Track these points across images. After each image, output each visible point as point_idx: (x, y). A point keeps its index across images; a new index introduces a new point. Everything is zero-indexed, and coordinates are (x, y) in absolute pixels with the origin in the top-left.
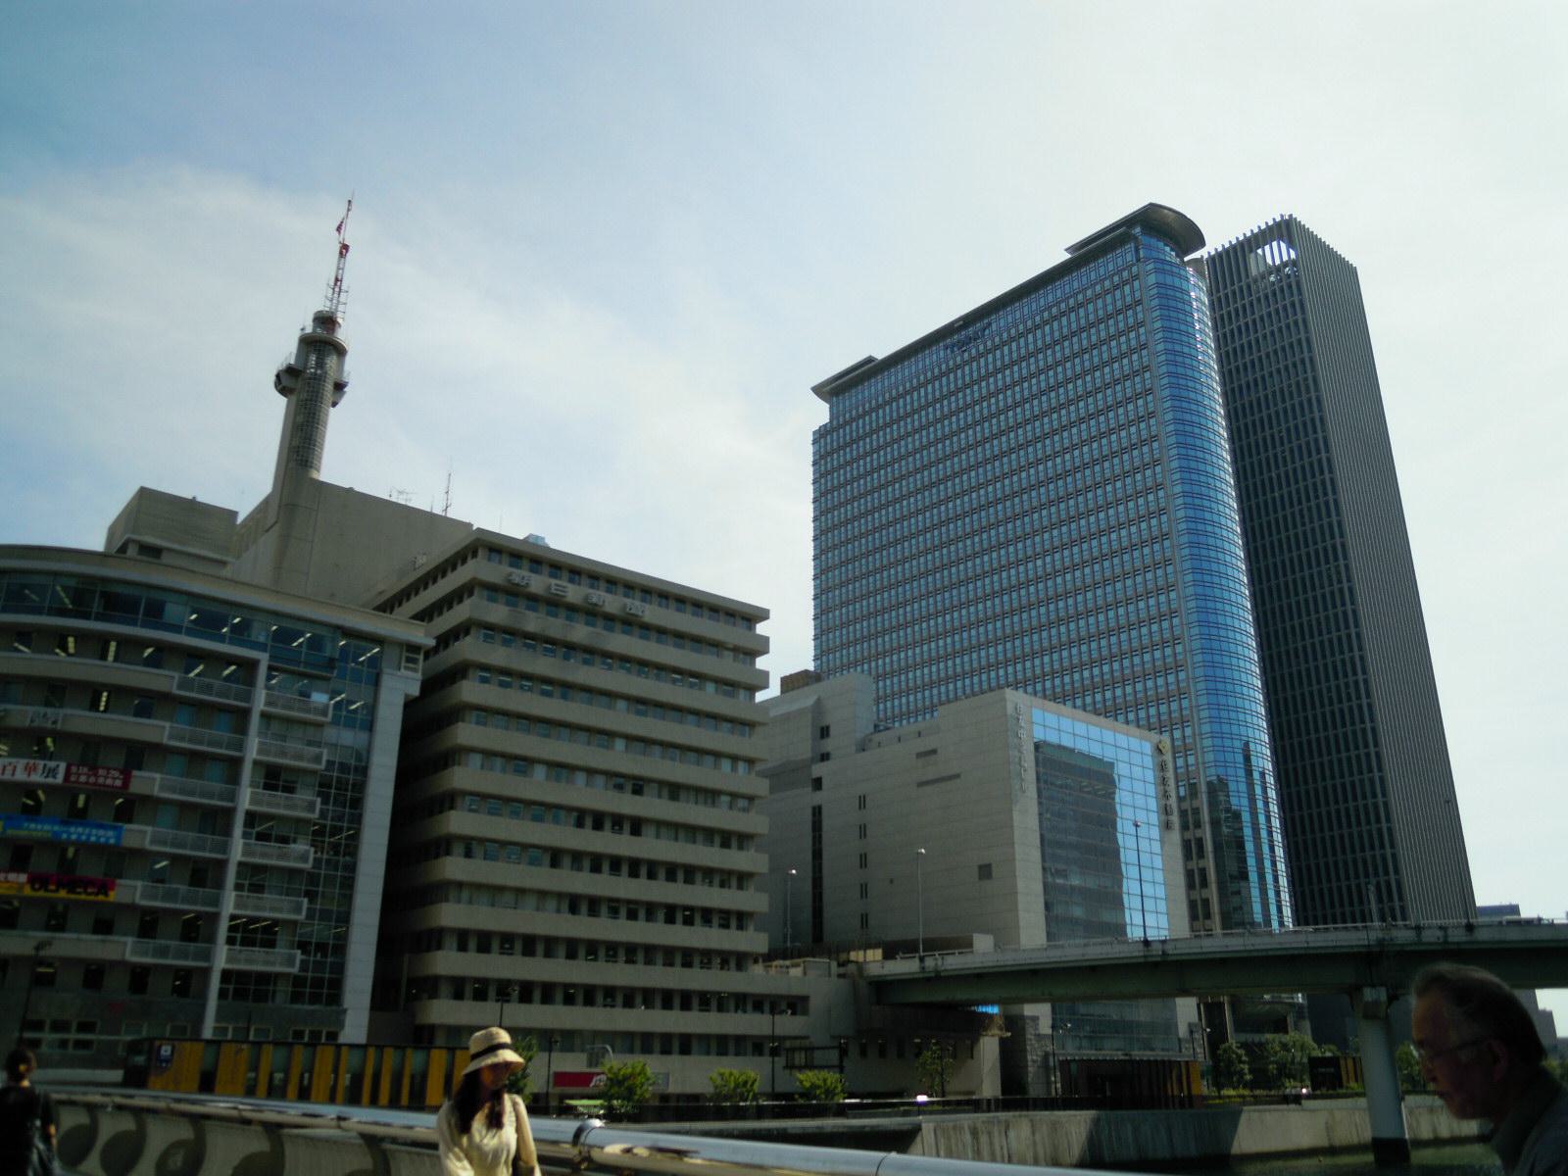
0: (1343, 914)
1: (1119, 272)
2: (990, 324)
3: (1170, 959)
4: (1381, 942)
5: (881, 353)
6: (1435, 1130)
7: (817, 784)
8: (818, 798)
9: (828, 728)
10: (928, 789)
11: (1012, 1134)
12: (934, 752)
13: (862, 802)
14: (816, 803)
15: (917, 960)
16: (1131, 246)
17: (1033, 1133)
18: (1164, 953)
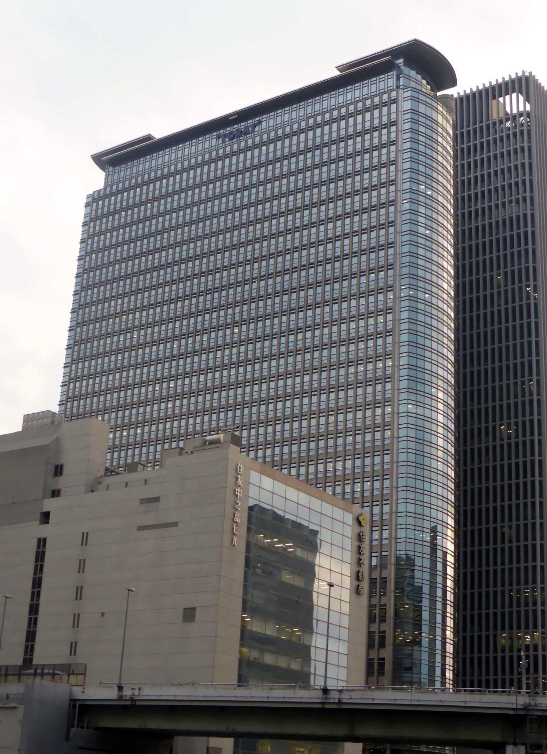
2: (260, 122)
4: (526, 708)
5: (159, 134)
7: (45, 517)
8: (44, 531)
9: (62, 466)
12: (156, 499)
13: (85, 538)
18: (340, 702)
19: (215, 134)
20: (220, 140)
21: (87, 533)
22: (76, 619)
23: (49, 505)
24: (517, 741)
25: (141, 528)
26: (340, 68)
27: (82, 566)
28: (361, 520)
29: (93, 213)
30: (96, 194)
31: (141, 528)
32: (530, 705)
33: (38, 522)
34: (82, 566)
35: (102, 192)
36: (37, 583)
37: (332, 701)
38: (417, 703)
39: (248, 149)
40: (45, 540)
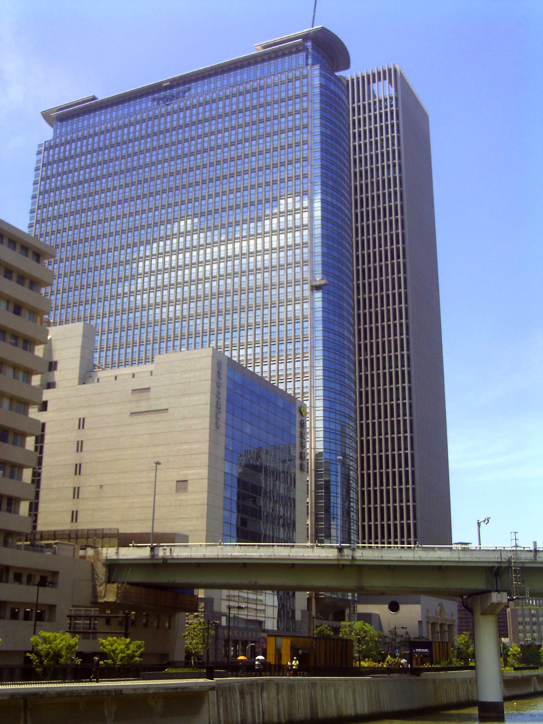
1: (94, 126)
2: (189, 89)
3: (357, 563)
5: (101, 96)
6: (313, 705)
9: (56, 363)
10: (140, 418)
11: (265, 695)
13: (82, 424)
15: (148, 549)
16: (302, 55)
17: (278, 693)
18: (353, 558)
19: (150, 97)
20: (155, 103)
21: (84, 419)
22: (76, 492)
24: (499, 588)
27: (80, 446)
29: (45, 160)
30: (47, 144)
34: (80, 446)
35: (52, 142)
37: (346, 558)
38: (478, 560)
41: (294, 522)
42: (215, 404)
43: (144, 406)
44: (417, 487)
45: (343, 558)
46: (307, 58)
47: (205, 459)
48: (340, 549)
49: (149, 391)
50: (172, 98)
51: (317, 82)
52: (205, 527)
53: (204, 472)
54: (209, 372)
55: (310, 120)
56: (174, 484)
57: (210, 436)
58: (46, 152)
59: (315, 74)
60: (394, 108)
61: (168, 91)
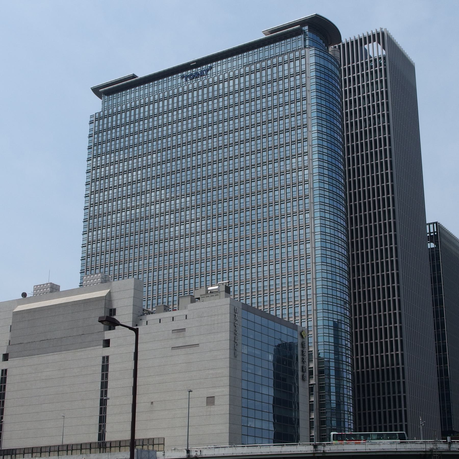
0: (396, 426)
2: (211, 68)
4: (431, 450)
5: (141, 75)
7: (107, 343)
8: (106, 352)
9: (115, 310)
12: (184, 330)
14: (105, 354)
16: (302, 36)
18: (324, 452)
19: (180, 74)
20: (184, 79)
23: (109, 335)
25: (173, 348)
26: (264, 33)
28: (303, 334)
29: (96, 128)
31: (173, 348)
32: (433, 449)
33: (102, 346)
35: (102, 113)
36: (104, 385)
37: (319, 452)
39: (204, 86)
40: (108, 357)
41: (298, 420)
42: (233, 340)
43: (180, 342)
44: (407, 381)
45: (317, 452)
46: (305, 40)
47: (226, 381)
48: (315, 446)
49: (185, 331)
50: (197, 76)
51: (312, 60)
52: (228, 430)
53: (226, 390)
54: (228, 316)
55: (308, 93)
56: (205, 400)
57: (230, 363)
58: (97, 122)
59: (311, 58)
60: (382, 67)
61: (194, 70)
